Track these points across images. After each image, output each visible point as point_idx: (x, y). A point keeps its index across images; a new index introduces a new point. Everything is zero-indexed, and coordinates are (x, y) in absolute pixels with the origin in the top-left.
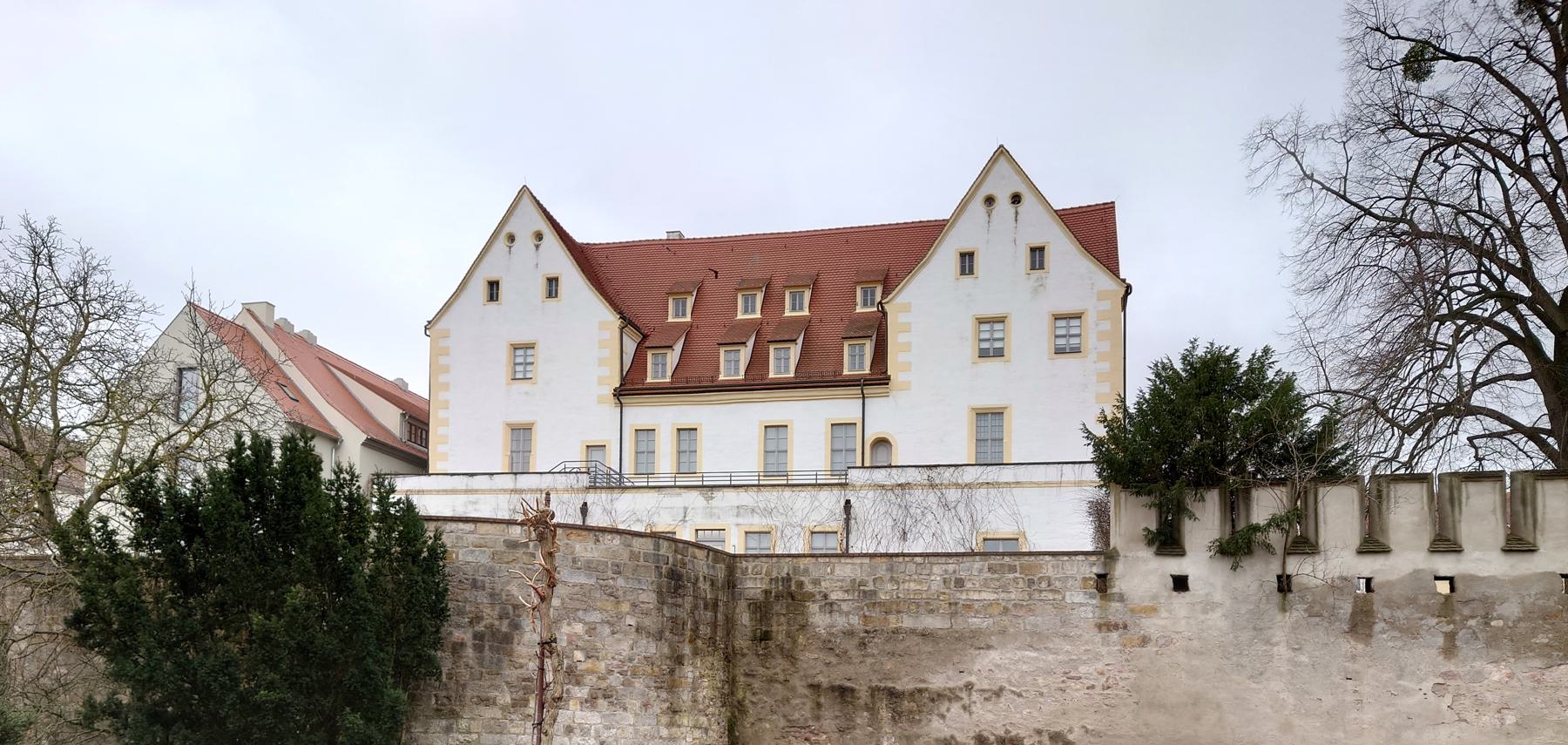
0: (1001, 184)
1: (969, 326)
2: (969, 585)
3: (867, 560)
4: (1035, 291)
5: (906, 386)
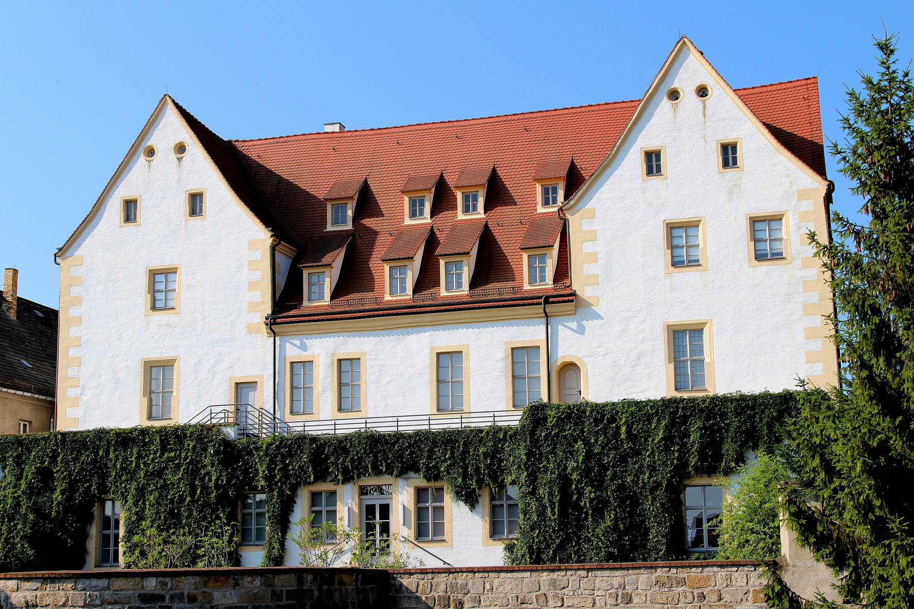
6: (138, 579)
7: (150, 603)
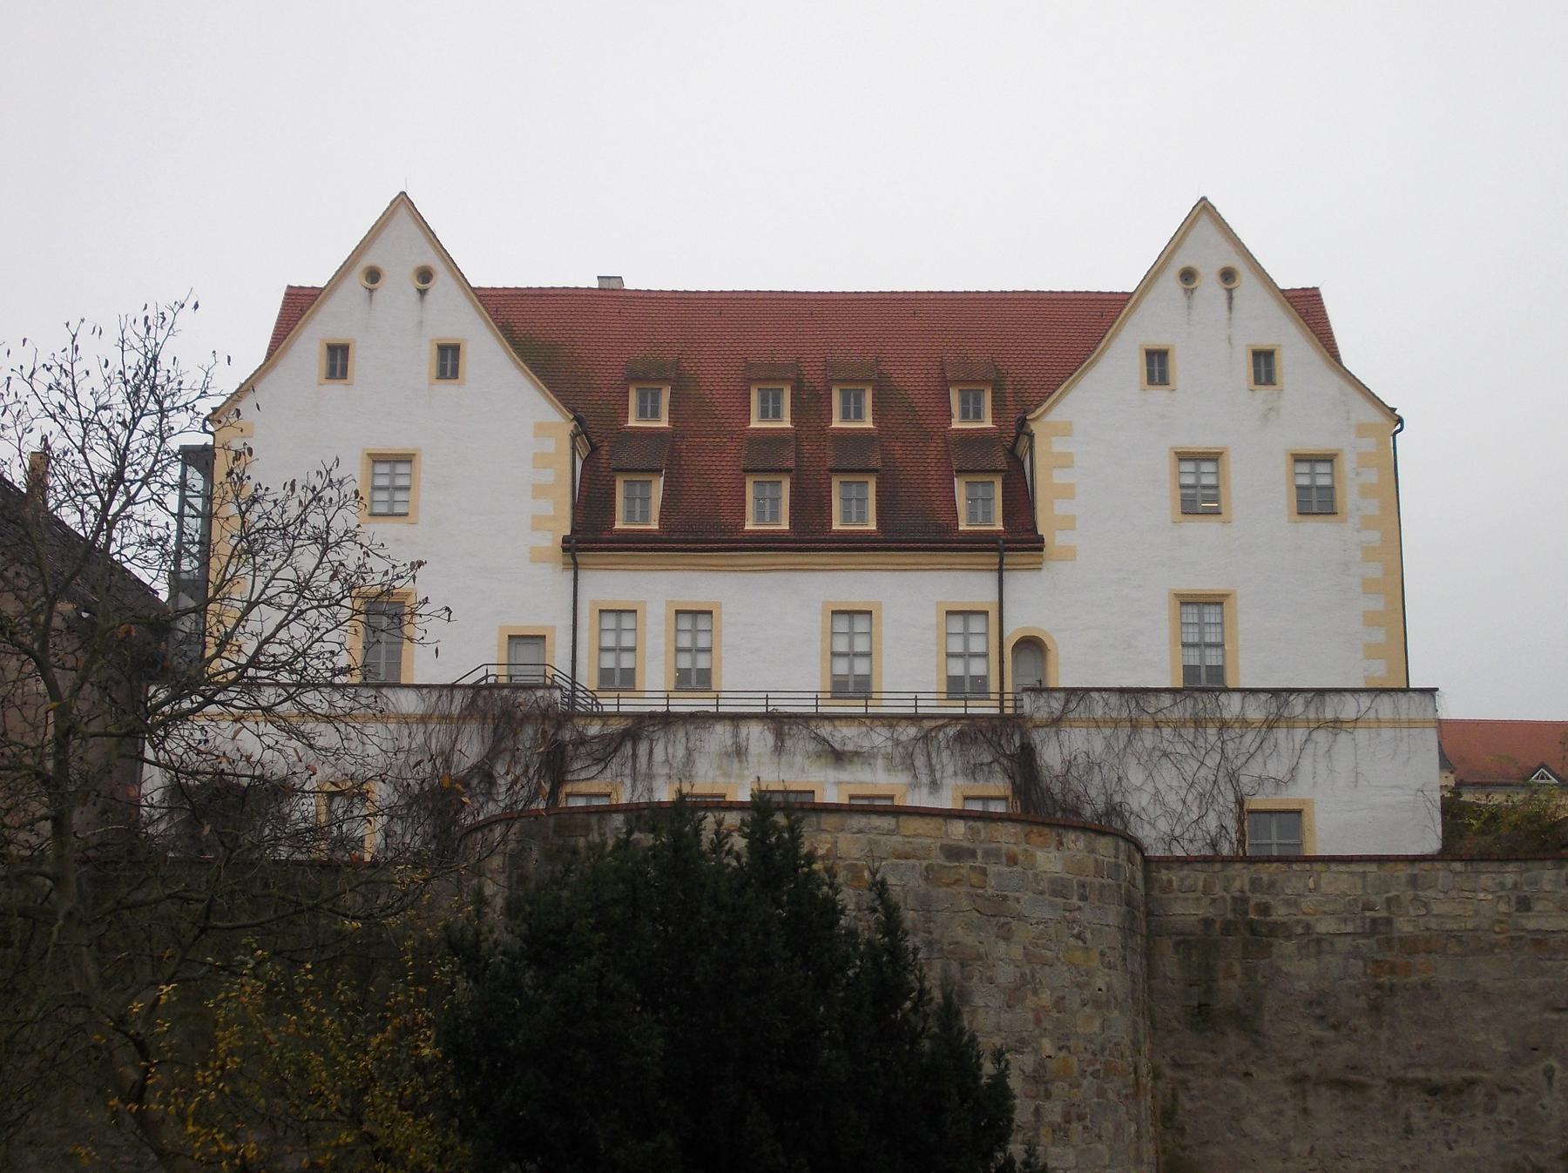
0: (1206, 253)
1: (1164, 465)
2: (1539, 906)
3: (1373, 867)
4: (1265, 418)
5: (1069, 554)
6: (941, 820)
7: (958, 860)
